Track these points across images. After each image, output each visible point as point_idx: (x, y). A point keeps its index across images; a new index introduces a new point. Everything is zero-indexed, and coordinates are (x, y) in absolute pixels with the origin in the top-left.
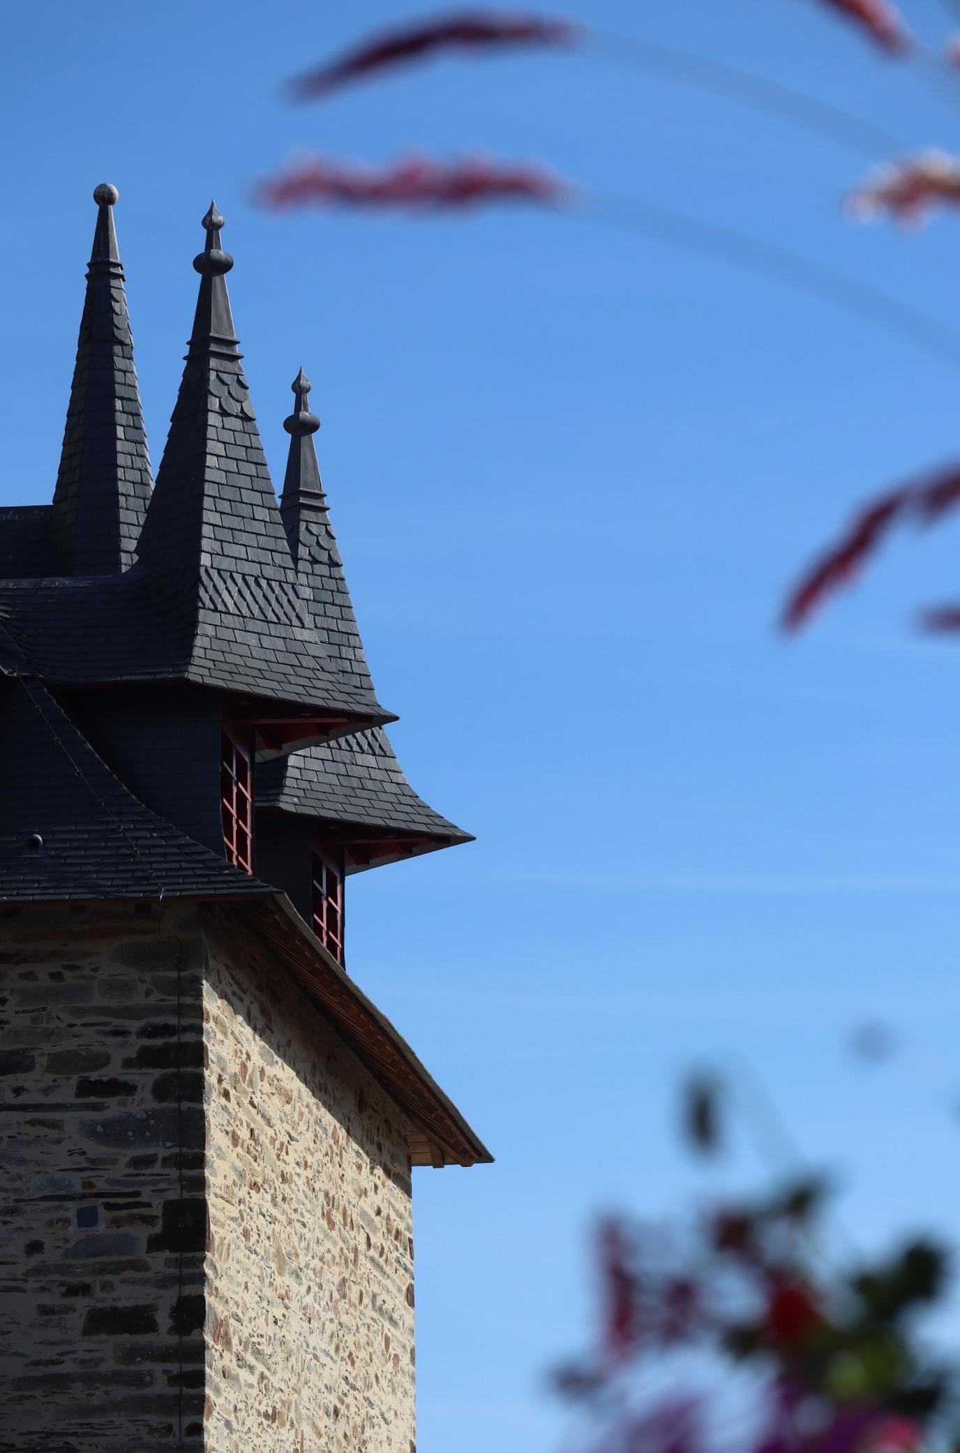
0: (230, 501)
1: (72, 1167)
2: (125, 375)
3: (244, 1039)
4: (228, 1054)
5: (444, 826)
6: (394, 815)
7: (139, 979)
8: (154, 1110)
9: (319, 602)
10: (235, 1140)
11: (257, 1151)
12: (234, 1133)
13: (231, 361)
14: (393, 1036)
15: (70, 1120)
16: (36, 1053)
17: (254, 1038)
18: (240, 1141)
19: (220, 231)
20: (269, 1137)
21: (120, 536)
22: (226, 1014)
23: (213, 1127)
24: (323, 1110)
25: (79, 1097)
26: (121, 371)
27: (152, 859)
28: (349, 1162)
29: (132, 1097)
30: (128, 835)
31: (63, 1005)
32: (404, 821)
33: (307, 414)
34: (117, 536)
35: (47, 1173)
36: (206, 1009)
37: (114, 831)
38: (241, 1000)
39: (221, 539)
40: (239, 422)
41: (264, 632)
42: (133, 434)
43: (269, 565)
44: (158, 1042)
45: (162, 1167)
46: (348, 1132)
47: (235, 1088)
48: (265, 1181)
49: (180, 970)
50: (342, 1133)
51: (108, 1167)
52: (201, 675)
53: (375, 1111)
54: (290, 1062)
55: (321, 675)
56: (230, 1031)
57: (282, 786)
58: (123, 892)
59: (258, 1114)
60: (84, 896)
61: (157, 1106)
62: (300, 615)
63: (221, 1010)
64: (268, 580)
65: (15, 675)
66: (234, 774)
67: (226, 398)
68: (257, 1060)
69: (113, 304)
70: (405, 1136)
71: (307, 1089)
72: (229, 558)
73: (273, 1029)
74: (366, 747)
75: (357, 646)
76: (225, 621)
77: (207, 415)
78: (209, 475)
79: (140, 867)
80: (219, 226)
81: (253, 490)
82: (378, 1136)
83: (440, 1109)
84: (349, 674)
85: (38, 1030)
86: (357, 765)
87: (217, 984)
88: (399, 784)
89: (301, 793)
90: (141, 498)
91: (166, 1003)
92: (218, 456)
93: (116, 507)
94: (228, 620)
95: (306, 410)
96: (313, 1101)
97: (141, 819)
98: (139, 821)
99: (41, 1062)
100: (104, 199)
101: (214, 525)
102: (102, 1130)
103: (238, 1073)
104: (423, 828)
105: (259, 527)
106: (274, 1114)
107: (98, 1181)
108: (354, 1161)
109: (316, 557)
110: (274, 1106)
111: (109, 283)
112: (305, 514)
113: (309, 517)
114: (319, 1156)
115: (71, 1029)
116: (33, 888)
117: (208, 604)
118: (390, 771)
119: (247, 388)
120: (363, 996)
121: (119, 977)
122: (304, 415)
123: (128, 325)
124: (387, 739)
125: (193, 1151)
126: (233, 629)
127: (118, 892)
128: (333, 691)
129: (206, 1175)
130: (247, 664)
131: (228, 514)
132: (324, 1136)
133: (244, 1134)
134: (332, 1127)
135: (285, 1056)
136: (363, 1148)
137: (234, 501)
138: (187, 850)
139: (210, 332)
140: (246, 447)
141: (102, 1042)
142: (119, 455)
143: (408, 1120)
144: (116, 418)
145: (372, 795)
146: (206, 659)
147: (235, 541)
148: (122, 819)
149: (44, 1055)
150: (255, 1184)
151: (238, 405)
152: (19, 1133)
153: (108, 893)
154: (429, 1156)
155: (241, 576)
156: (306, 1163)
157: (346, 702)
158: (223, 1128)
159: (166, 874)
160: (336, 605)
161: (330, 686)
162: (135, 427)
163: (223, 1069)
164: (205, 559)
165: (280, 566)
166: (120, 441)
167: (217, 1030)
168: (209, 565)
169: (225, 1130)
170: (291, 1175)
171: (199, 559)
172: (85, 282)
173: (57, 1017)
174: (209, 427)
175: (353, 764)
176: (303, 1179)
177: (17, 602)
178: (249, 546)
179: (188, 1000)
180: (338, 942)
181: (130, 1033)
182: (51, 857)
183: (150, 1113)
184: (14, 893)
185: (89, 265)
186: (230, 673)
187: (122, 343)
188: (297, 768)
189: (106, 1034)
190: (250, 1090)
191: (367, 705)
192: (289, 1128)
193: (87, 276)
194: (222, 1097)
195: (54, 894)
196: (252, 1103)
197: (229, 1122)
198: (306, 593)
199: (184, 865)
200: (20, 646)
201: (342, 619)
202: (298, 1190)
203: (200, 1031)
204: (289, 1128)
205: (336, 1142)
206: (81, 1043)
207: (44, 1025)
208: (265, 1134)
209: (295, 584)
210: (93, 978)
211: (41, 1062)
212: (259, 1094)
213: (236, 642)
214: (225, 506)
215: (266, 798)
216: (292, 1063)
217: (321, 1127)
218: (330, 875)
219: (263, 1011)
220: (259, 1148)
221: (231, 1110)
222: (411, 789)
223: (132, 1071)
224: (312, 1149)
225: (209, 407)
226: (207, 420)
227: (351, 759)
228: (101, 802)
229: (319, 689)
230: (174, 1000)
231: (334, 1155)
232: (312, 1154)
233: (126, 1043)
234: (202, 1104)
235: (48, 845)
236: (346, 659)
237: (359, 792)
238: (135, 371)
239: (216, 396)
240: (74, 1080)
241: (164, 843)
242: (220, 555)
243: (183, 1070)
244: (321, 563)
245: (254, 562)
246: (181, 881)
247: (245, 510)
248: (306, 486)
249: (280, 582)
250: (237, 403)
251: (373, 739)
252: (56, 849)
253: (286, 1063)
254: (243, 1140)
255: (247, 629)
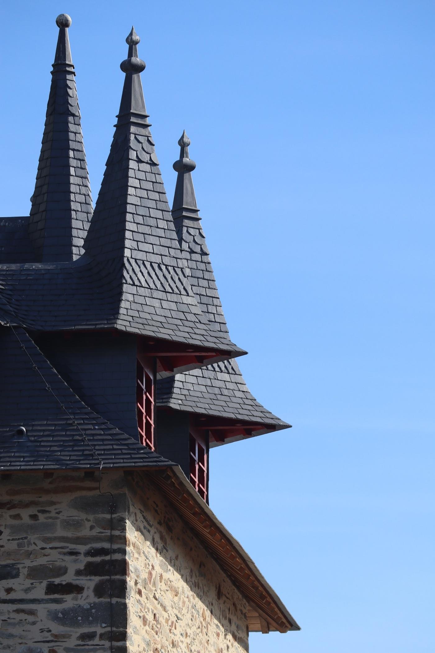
0: (143, 216)
1: (43, 640)
2: (75, 135)
3: (150, 556)
4: (141, 566)
5: (272, 419)
6: (241, 411)
7: (86, 519)
8: (95, 603)
9: (195, 277)
10: (145, 621)
11: (158, 628)
12: (144, 617)
13: (144, 128)
14: (241, 552)
15: (42, 610)
16: (20, 566)
17: (157, 555)
18: (148, 622)
19: (137, 46)
20: (165, 618)
21: (72, 236)
22: (140, 541)
23: (131, 614)
24: (197, 599)
25: (47, 595)
26: (73, 132)
27: (95, 443)
28: (212, 631)
29: (81, 595)
30: (80, 427)
31: (39, 536)
32: (247, 415)
33: (188, 159)
34: (70, 237)
35: (26, 644)
36: (128, 538)
37: (71, 425)
38: (149, 531)
39: (137, 240)
40: (148, 166)
41: (164, 299)
42: (80, 172)
43: (167, 256)
44: (98, 559)
45: (100, 640)
46: (212, 612)
47: (145, 588)
48: (162, 647)
49: (112, 513)
50: (208, 613)
51: (65, 640)
52: (125, 326)
53: (227, 598)
54: (177, 570)
55: (198, 325)
56: (142, 552)
57: (171, 393)
58: (77, 464)
59: (158, 604)
60: (52, 467)
61: (97, 600)
62: (186, 288)
63: (137, 538)
64: (166, 266)
65: (8, 325)
66: (144, 387)
67: (141, 152)
68: (158, 569)
69: (68, 90)
70: (245, 613)
71: (187, 586)
72: (142, 252)
73: (168, 549)
74: (223, 368)
75: (218, 305)
76: (139, 291)
77: (128, 162)
78: (130, 199)
79: (87, 448)
80: (137, 43)
81: (157, 209)
82: (229, 614)
83: (268, 597)
84: (213, 323)
85: (21, 552)
86: (218, 380)
87: (135, 522)
88: (244, 392)
89: (183, 397)
90: (85, 213)
91: (103, 534)
92: (135, 188)
93: (70, 218)
94: (141, 291)
95: (187, 157)
96: (191, 593)
97: (88, 417)
98: (87, 419)
99: (24, 572)
100: (63, 24)
101: (133, 231)
102: (62, 616)
103: (147, 578)
104: (259, 420)
105: (161, 233)
106: (168, 603)
107: (59, 649)
108: (215, 631)
109: (193, 249)
110: (168, 598)
111: (66, 77)
112: (186, 222)
113: (188, 224)
114: (194, 628)
115: (43, 551)
116: (20, 461)
117: (129, 281)
118: (238, 383)
119: (153, 145)
120: (224, 528)
121: (74, 518)
122: (186, 160)
123: (77, 104)
124: (236, 364)
125: (118, 630)
126: (144, 296)
127: (74, 464)
128: (206, 335)
129: (127, 645)
130: (153, 318)
131: (142, 224)
132: (197, 616)
133: (150, 617)
134: (202, 610)
135: (174, 565)
136: (220, 622)
137: (145, 216)
138: (117, 437)
139: (131, 110)
140: (153, 182)
141: (62, 559)
142: (72, 186)
143: (247, 604)
144: (70, 162)
145: (227, 399)
146: (128, 315)
147: (146, 241)
148: (76, 417)
149: (26, 567)
150: (156, 649)
151: (148, 155)
152: (9, 618)
153: (67, 465)
154: (259, 626)
155: (150, 263)
156: (187, 634)
157: (215, 343)
158: (137, 614)
159: (104, 453)
160: (205, 279)
161: (204, 333)
162: (81, 168)
163: (138, 576)
164: (127, 253)
165: (174, 257)
166: (73, 177)
167: (134, 551)
168: (130, 256)
169: (139, 616)
170: (178, 642)
171: (123, 252)
172: (51, 76)
173: (34, 543)
174: (130, 169)
175: (215, 379)
176: (185, 644)
177: (9, 278)
178: (155, 245)
179: (117, 533)
180: (205, 490)
181: (80, 553)
182: (31, 441)
183: (92, 605)
184: (8, 465)
185: (53, 65)
186: (143, 324)
187: (74, 115)
188: (181, 382)
189: (65, 554)
190: (154, 589)
191: (228, 345)
192: (176, 612)
193: (52, 73)
194: (137, 594)
195: (33, 465)
196: (155, 597)
197: (141, 610)
198: (188, 272)
199: (115, 447)
200: (11, 307)
201: (209, 288)
202: (182, 652)
203: (124, 552)
204: (176, 612)
205: (204, 619)
206: (49, 560)
207: (26, 548)
208: (162, 616)
209: (183, 268)
210: (57, 518)
211: (24, 572)
212: (159, 591)
213: (146, 305)
214: (139, 219)
215: (161, 401)
216: (178, 570)
217: (196, 610)
218: (200, 447)
219: (162, 538)
220: (159, 626)
221: (142, 602)
222: (251, 395)
223: (81, 578)
224: (190, 624)
225: (130, 157)
226: (129, 165)
227: (214, 376)
228: (62, 406)
229: (198, 334)
230: (108, 532)
231: (203, 627)
232: (190, 628)
233: (77, 560)
234: (125, 599)
235: (29, 434)
236: (211, 313)
237: (219, 397)
238: (82, 133)
239: (134, 150)
240: (45, 584)
241: (103, 433)
242: (136, 250)
243: (113, 577)
244: (196, 253)
245: (158, 254)
246: (114, 457)
247: (152, 222)
248: (187, 204)
249: (174, 267)
250: (147, 155)
251: (228, 364)
252: (34, 436)
253: (175, 570)
254: (150, 621)
255: (153, 297)
